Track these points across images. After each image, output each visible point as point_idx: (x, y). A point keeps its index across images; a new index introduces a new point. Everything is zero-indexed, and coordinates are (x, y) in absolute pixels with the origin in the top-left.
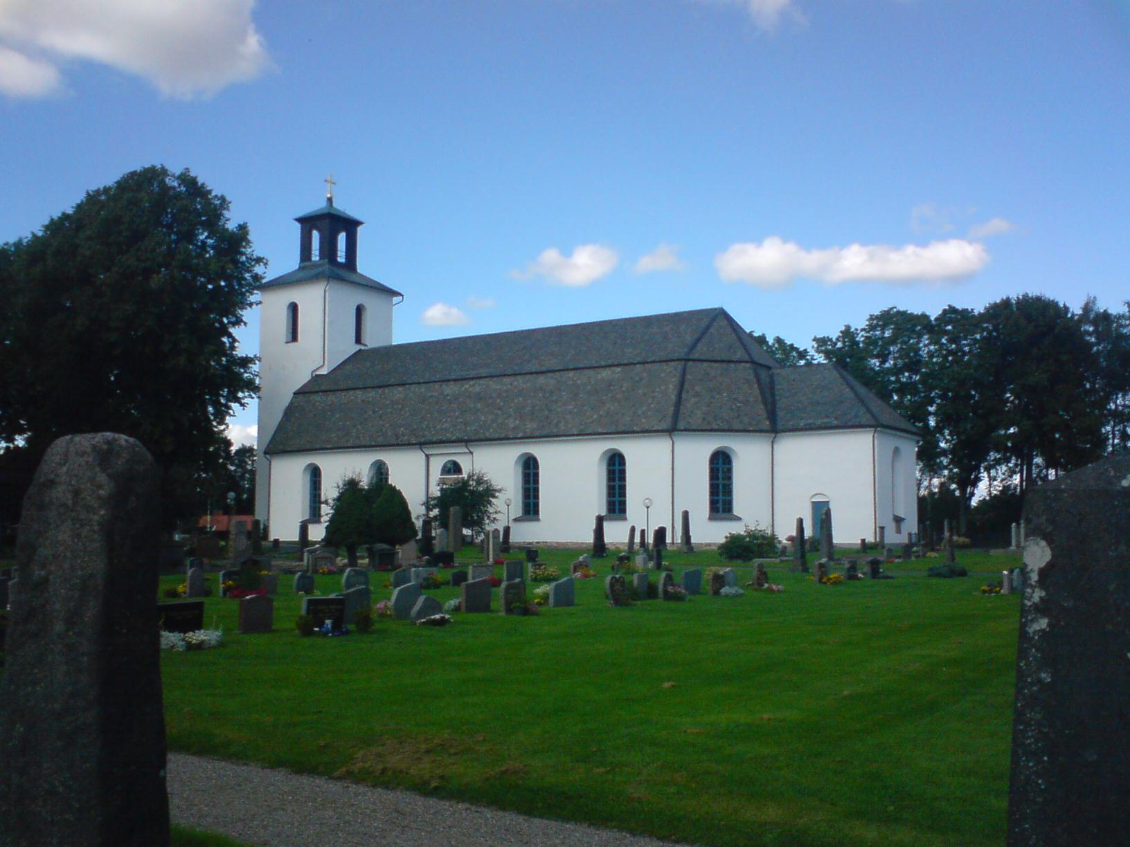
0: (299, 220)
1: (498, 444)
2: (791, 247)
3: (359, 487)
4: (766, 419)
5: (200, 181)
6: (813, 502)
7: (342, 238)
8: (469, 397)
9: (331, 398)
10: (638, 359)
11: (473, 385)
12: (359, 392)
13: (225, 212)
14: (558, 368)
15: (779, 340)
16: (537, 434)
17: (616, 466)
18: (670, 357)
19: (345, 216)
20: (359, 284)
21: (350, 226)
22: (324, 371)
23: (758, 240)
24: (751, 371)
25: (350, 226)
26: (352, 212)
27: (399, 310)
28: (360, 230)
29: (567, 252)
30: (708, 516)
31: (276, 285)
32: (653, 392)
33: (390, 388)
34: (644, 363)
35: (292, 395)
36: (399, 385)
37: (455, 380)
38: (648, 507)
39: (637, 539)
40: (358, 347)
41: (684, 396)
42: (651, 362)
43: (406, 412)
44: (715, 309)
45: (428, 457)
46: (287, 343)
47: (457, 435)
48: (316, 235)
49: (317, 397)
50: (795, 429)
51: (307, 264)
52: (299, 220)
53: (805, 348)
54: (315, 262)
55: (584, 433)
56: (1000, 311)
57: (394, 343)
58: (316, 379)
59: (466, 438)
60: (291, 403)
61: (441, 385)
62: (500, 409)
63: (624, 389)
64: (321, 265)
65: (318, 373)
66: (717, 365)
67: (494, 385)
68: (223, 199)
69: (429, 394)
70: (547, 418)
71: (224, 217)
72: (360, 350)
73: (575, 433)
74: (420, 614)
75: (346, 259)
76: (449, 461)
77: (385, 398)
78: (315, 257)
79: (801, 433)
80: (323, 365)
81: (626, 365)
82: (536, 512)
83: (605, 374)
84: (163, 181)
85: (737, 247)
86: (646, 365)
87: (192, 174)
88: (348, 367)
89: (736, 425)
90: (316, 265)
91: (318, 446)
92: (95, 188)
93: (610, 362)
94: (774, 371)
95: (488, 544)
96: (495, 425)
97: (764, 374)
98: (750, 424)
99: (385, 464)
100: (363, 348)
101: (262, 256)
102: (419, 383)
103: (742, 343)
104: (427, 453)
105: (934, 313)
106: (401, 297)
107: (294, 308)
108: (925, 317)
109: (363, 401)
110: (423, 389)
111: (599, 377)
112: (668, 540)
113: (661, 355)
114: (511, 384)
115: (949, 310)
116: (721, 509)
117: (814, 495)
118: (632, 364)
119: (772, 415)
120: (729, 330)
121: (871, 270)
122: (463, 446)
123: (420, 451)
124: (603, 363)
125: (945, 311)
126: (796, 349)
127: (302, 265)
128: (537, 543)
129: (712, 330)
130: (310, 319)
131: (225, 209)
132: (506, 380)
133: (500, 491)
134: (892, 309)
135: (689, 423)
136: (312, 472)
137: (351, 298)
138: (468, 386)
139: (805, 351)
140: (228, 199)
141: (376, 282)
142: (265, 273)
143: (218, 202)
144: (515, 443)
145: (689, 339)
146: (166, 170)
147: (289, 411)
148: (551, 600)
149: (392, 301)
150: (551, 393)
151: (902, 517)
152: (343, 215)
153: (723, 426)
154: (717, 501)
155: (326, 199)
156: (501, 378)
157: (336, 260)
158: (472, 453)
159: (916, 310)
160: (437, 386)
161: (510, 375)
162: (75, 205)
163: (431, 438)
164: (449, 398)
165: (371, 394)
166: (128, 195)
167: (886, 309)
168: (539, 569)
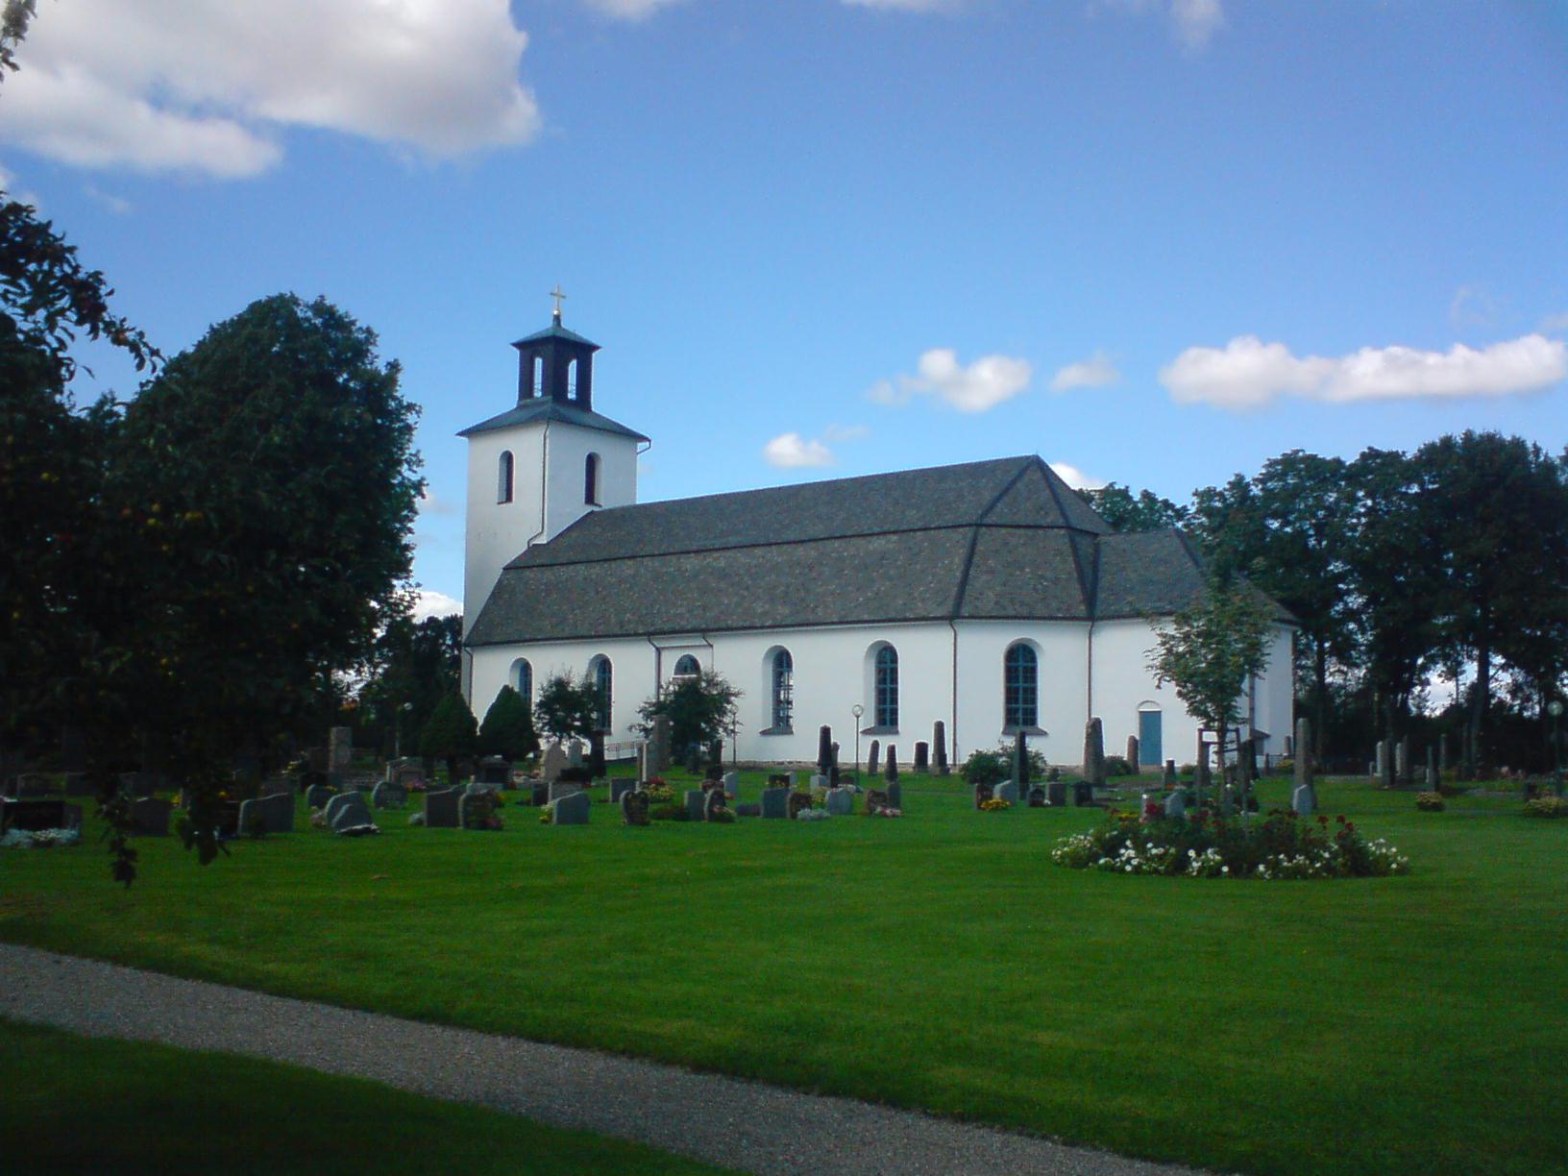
0: (519, 345)
1: (561, 645)
2: (1276, 353)
3: (570, 689)
4: (1080, 602)
5: (341, 310)
6: (1141, 712)
8: (711, 573)
9: (548, 575)
10: (920, 525)
11: (718, 558)
12: (581, 567)
14: (822, 536)
15: (1147, 496)
16: (789, 621)
17: (886, 664)
18: (960, 521)
19: (577, 340)
20: (593, 428)
21: (583, 351)
22: (543, 540)
23: (1220, 344)
24: (1066, 540)
25: (583, 351)
26: (585, 332)
27: (645, 459)
29: (965, 360)
30: (1001, 729)
31: (484, 430)
32: (934, 567)
33: (619, 561)
34: (925, 529)
35: (502, 570)
36: (629, 558)
37: (696, 552)
38: (858, 717)
39: (883, 758)
40: (589, 509)
41: (972, 572)
42: (935, 528)
43: (635, 593)
44: (1027, 458)
45: (659, 651)
46: (499, 503)
47: (694, 623)
48: (539, 362)
50: (1102, 619)
52: (519, 345)
53: (1184, 504)
54: (537, 398)
55: (846, 622)
56: (1438, 455)
57: (639, 502)
58: (534, 549)
59: (704, 626)
60: (500, 581)
61: (679, 559)
62: (747, 589)
63: (899, 563)
64: (542, 403)
65: (537, 542)
66: (1022, 531)
67: (741, 558)
68: (369, 331)
69: (665, 570)
70: (803, 600)
71: (372, 354)
72: (592, 512)
73: (835, 620)
74: (341, 824)
75: (577, 394)
76: (685, 656)
77: (611, 575)
78: (538, 394)
79: (1127, 621)
80: (542, 532)
81: (903, 531)
82: (894, 722)
83: (878, 544)
85: (1193, 353)
86: (929, 532)
87: (328, 302)
88: (574, 535)
89: (1040, 610)
90: (539, 403)
91: (527, 636)
93: (885, 528)
94: (1102, 539)
95: (641, 764)
96: (740, 610)
97: (1085, 543)
98: (1059, 610)
99: (788, 654)
100: (596, 509)
101: (414, 402)
102: (653, 556)
103: (1058, 502)
104: (658, 646)
105: (1350, 458)
106: (648, 443)
108: (1338, 462)
109: (585, 579)
110: (657, 563)
111: (871, 547)
112: (949, 761)
113: (949, 518)
114: (763, 557)
115: (1369, 453)
116: (1021, 721)
117: (1143, 703)
118: (910, 530)
119: (1090, 600)
120: (1043, 484)
121: (1395, 384)
122: (644, 640)
123: (949, 627)
124: (877, 530)
125: (1363, 455)
126: (1171, 506)
127: (522, 403)
128: (790, 763)
129: (1019, 485)
131: (371, 344)
132: (758, 551)
133: (736, 695)
134: (1298, 451)
135: (977, 607)
136: (601, 664)
137: (578, 445)
138: (711, 560)
139: (1185, 508)
140: (376, 331)
141: (614, 423)
142: (416, 423)
143: (364, 336)
144: (763, 634)
145: (987, 497)
146: (297, 299)
148: (555, 819)
149: (636, 448)
150: (811, 568)
151: (1267, 732)
153: (1025, 612)
154: (1016, 710)
155: (552, 318)
156: (751, 549)
158: (711, 646)
159: (1327, 454)
160: (674, 558)
161: (763, 545)
162: (196, 343)
163: (662, 626)
164: (687, 574)
165: (596, 570)
167: (1289, 452)
168: (648, 788)
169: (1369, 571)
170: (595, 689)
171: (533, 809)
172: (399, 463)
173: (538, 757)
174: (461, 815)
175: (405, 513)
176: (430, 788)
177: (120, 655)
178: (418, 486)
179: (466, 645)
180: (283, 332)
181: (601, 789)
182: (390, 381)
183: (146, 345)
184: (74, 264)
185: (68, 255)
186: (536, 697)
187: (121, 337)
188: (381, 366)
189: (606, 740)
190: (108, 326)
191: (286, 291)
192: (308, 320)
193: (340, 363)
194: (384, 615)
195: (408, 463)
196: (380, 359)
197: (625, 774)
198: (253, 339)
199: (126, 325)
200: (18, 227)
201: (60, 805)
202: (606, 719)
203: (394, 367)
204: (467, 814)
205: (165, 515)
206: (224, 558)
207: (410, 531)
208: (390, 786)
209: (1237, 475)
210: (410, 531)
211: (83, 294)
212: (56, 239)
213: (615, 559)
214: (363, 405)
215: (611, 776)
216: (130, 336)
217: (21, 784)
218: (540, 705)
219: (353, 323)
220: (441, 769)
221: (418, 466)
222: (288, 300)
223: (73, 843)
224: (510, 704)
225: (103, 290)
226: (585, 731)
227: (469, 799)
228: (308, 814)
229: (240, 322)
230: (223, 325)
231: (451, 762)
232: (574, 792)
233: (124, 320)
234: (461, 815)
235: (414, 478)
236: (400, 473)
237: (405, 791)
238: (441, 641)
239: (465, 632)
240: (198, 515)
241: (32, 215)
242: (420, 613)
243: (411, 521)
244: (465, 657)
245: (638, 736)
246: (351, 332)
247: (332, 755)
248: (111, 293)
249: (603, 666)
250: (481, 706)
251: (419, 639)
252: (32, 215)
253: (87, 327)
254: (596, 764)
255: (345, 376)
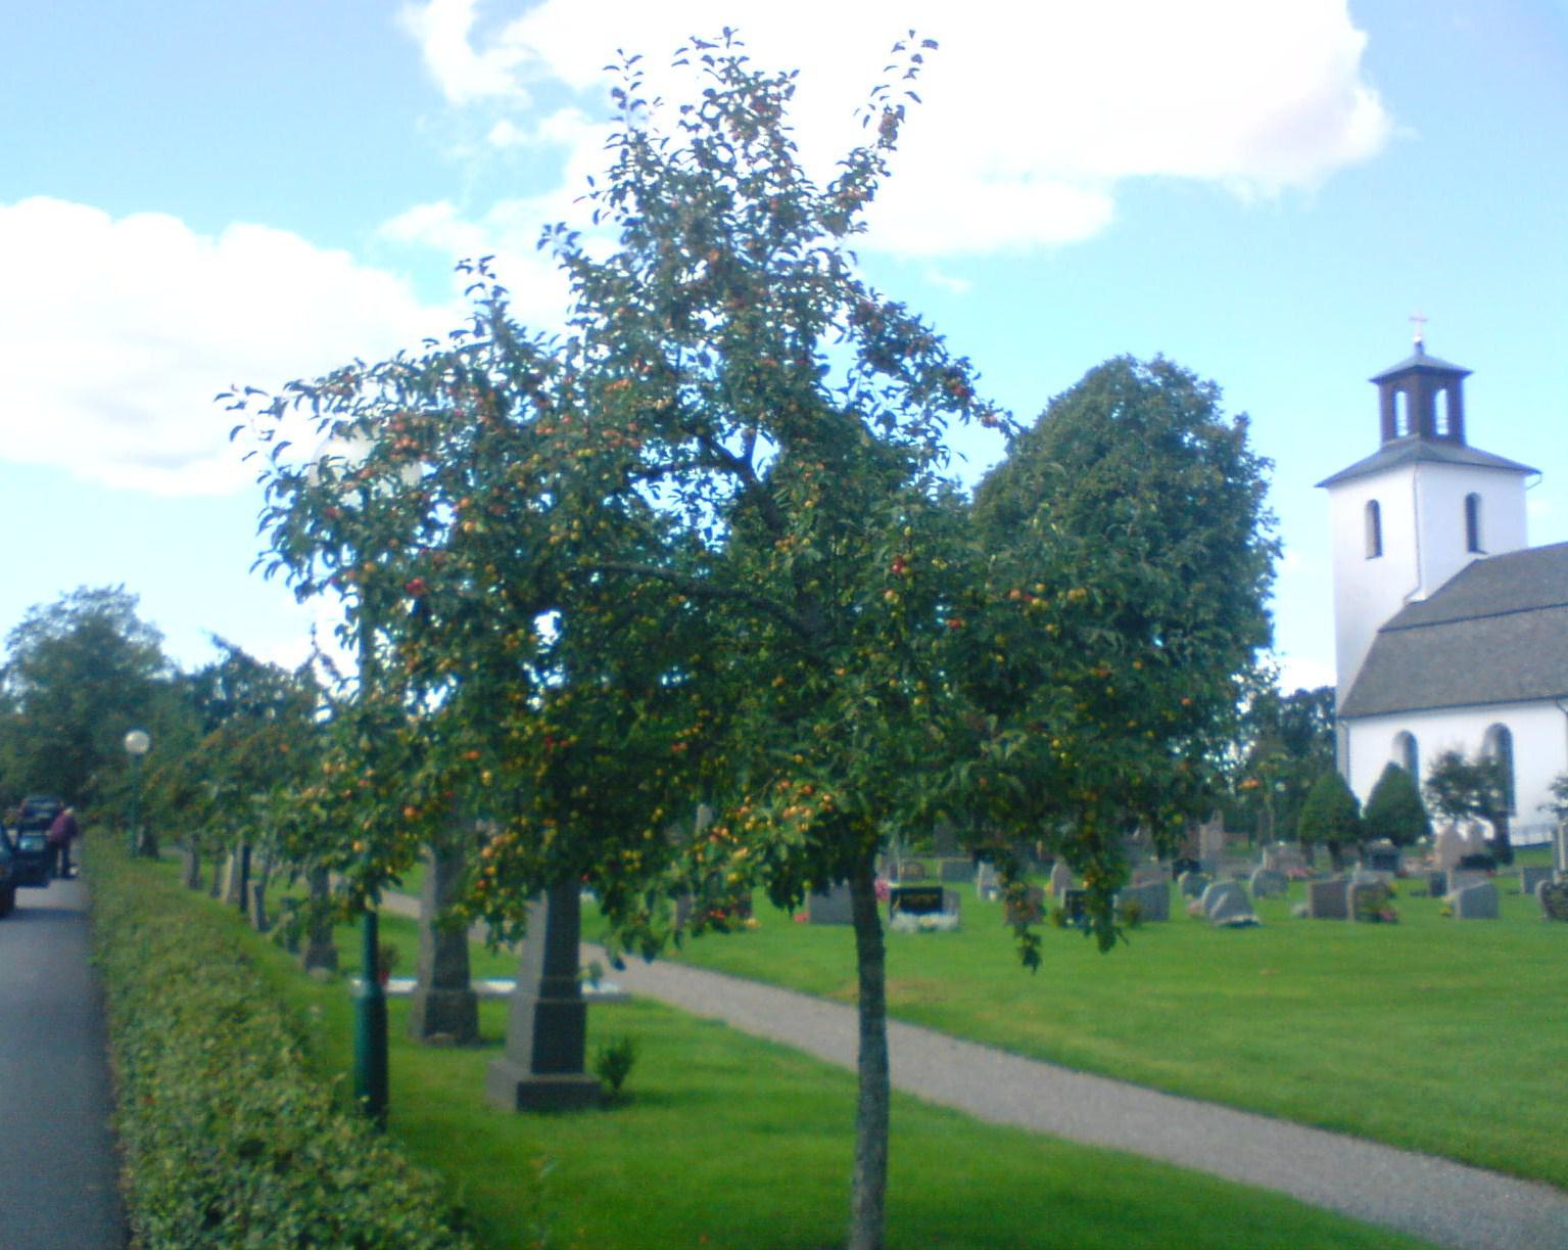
7: (1441, 399)
9: (1430, 636)
13: (1216, 402)
20: (1474, 464)
21: (1452, 379)
22: (1421, 596)
25: (1452, 379)
28: (1468, 384)
36: (1525, 610)
40: (1473, 557)
46: (1369, 558)
48: (1401, 398)
49: (1409, 635)
51: (1393, 442)
54: (1403, 437)
58: (1412, 608)
68: (1212, 386)
78: (1403, 432)
84: (1131, 375)
87: (1167, 359)
90: (1405, 443)
92: (1058, 393)
100: (1480, 557)
107: (1374, 508)
130: (1398, 527)
137: (1454, 486)
140: (1220, 384)
147: (1374, 658)
148: (1458, 911)
152: (1439, 366)
157: (1435, 433)
165: (1484, 627)
166: (1086, 400)
169: (656, 696)
170: (1494, 763)
171: (1429, 900)
172: (1254, 523)
173: (1431, 842)
174: (1350, 906)
175: (1263, 576)
176: (1313, 876)
177: (1017, 738)
178: (1276, 547)
179: (1342, 717)
180: (1123, 397)
181: (1508, 878)
182: (1239, 436)
183: (1015, 424)
184: (943, 352)
185: (937, 345)
186: (1424, 773)
187: (991, 418)
188: (1228, 421)
189: (1512, 822)
190: (979, 408)
191: (1122, 353)
192: (1148, 380)
193: (1184, 423)
194: (1248, 688)
195: (1263, 522)
196: (1226, 415)
197: (1539, 860)
198: (1094, 408)
199: (995, 406)
200: (894, 325)
201: (938, 891)
202: (1508, 798)
203: (1243, 420)
204: (1356, 906)
205: (1050, 593)
206: (1111, 636)
207: (1271, 595)
208: (1268, 874)
209: (293, 548)
210: (1271, 595)
211: (953, 381)
212: (927, 331)
213: (1508, 613)
214: (1213, 464)
215: (1520, 863)
216: (1000, 417)
217: (901, 870)
218: (1431, 783)
219: (1194, 378)
220: (1322, 853)
221: (1274, 523)
222: (1125, 362)
223: (956, 930)
224: (1396, 781)
225: (971, 375)
226: (1485, 811)
227: (1359, 889)
228: (1183, 904)
229: (1079, 391)
230: (1061, 396)
231: (1334, 847)
232: (1478, 880)
233: (992, 402)
234: (1350, 906)
235: (1271, 538)
236: (1255, 534)
237: (1284, 880)
238: (1311, 715)
239: (1338, 709)
240: (1082, 592)
241: (905, 311)
242: (1286, 688)
243: (1272, 584)
244: (1340, 732)
245: (1550, 817)
246: (1193, 388)
247: (1202, 841)
248: (978, 377)
249: (1502, 737)
250: (1363, 781)
251: (1288, 715)
252: (905, 311)
253: (959, 413)
254: (1500, 852)
255: (1191, 435)
